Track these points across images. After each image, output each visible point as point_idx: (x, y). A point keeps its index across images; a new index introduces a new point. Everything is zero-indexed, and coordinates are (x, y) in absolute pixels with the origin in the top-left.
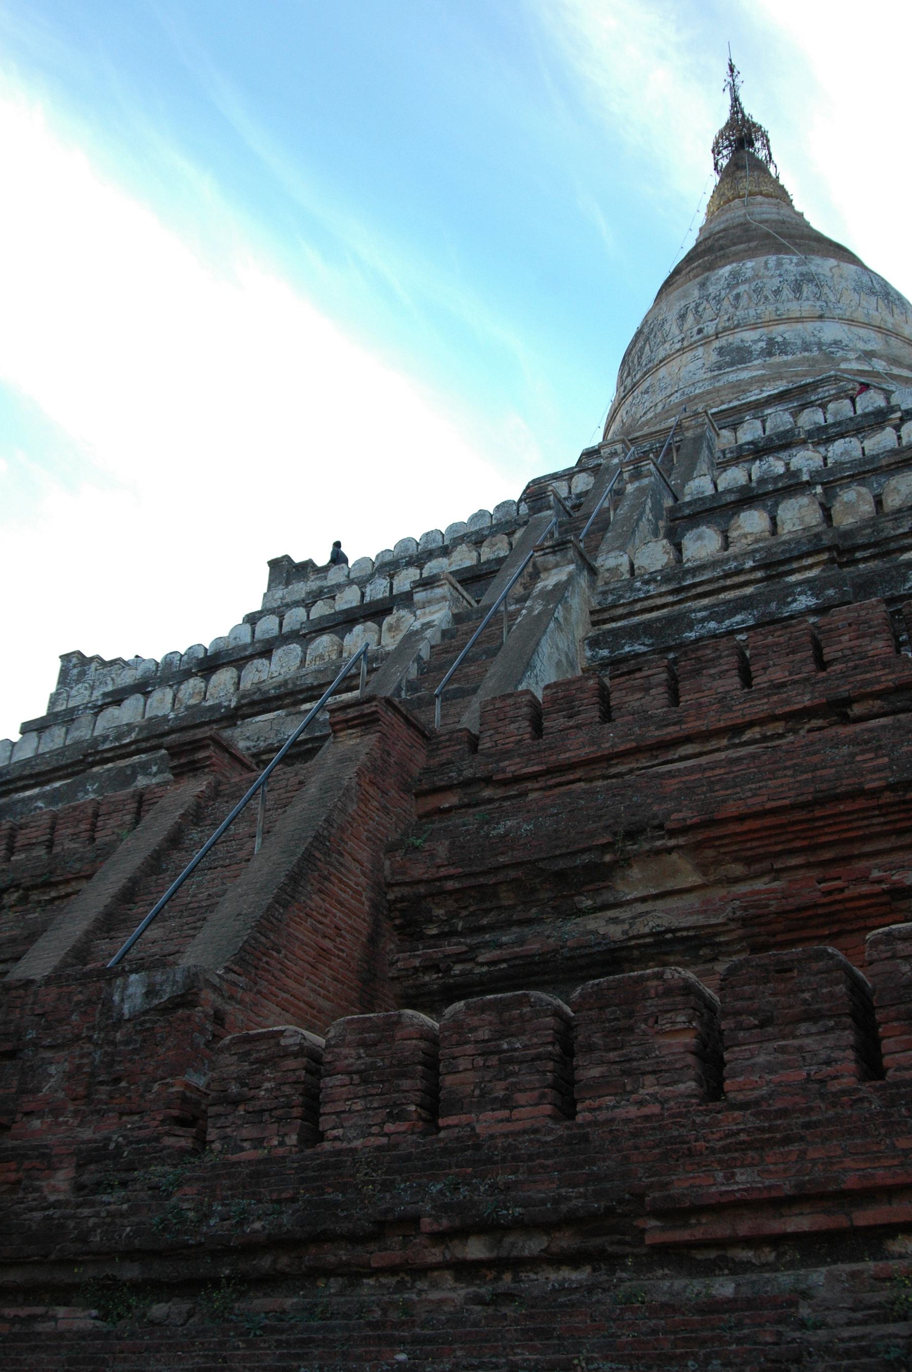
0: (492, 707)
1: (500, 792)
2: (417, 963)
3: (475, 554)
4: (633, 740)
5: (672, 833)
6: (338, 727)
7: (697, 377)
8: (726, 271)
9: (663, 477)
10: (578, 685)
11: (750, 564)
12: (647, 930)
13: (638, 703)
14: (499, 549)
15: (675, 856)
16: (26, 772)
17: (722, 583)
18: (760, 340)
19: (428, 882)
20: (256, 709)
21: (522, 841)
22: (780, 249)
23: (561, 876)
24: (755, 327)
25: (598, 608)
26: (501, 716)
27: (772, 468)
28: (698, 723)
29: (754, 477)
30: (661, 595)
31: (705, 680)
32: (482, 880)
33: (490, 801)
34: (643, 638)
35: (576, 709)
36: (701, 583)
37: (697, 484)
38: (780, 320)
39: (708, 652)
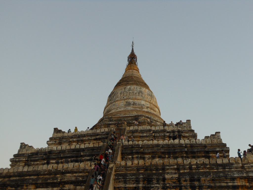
3: (93, 145)
7: (122, 106)
8: (129, 87)
11: (135, 168)
16: (27, 174)
18: (132, 102)
22: (137, 85)
24: (132, 99)
30: (124, 170)
38: (136, 99)
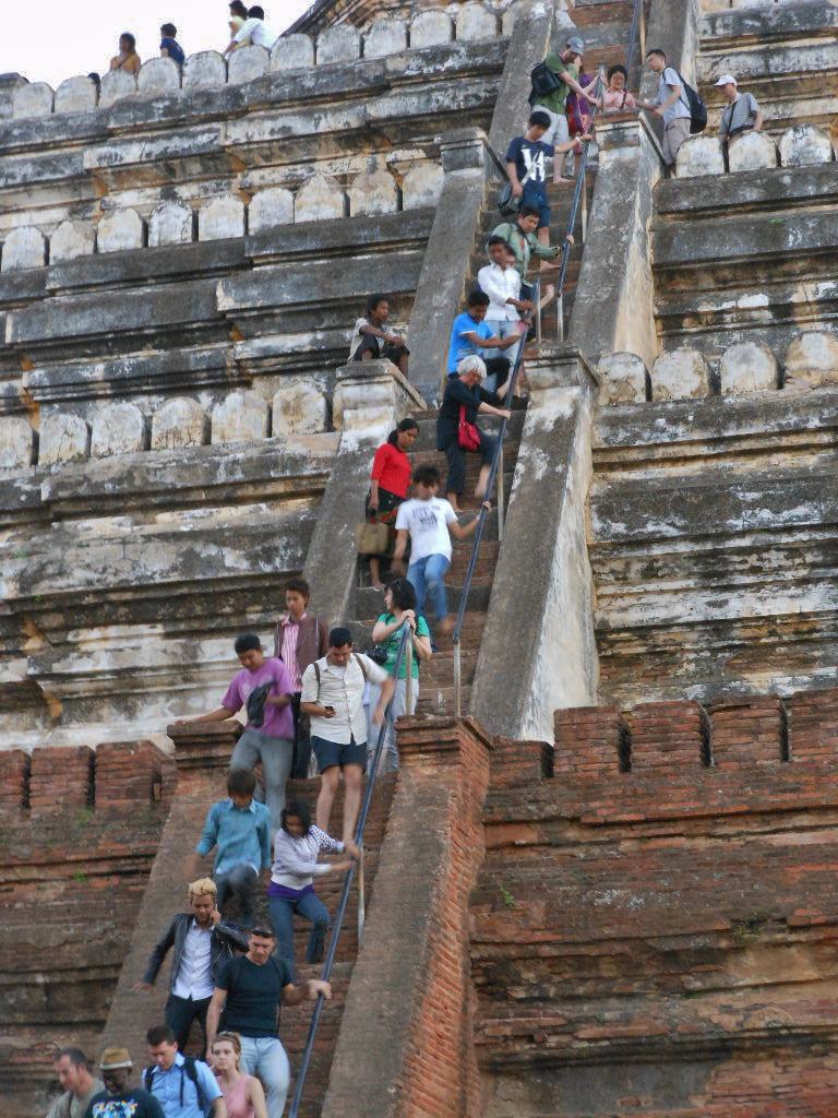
0: (569, 721)
1: (588, 835)
2: (508, 1031)
4: (745, 802)
5: (794, 929)
6: (407, 749)
9: (653, 143)
10: (675, 712)
11: (814, 423)
12: (762, 1024)
13: (744, 749)
14: (380, 196)
15: (793, 950)
17: (775, 441)
19: (520, 945)
20: (82, 507)
21: (630, 916)
23: (672, 955)
25: (604, 446)
26: (582, 735)
27: (812, 148)
28: (818, 795)
29: (784, 158)
30: (692, 443)
31: (822, 734)
32: (583, 950)
33: (576, 844)
34: (672, 515)
35: (673, 742)
36: (748, 437)
37: (697, 149)
39: (827, 700)
